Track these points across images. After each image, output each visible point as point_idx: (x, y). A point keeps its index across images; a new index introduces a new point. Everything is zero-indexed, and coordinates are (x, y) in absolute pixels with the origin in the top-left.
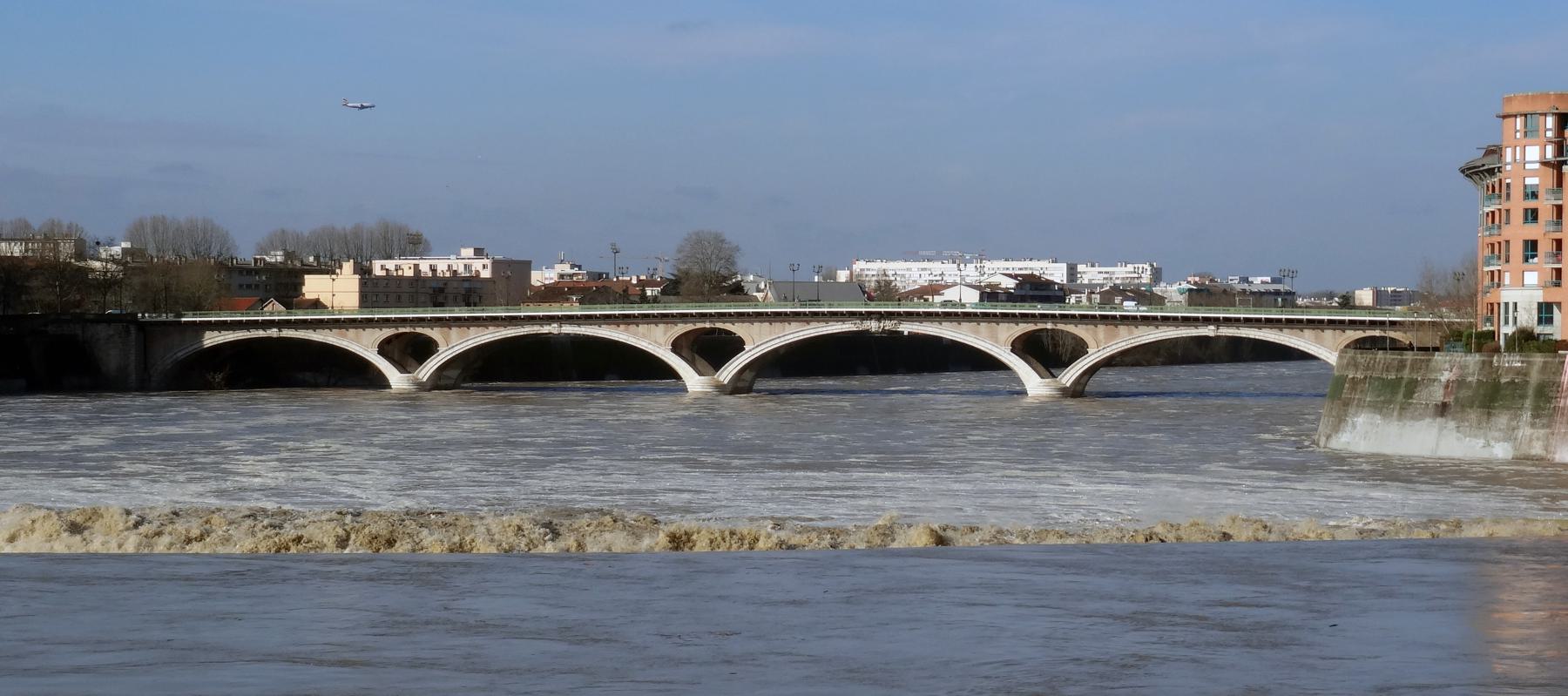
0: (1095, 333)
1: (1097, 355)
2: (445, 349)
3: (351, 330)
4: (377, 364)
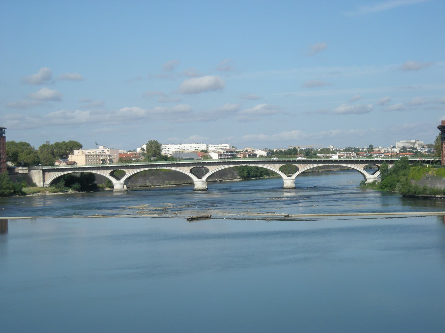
0: (301, 166)
1: (301, 171)
2: (128, 174)
3: (308, 164)
4: (110, 178)
